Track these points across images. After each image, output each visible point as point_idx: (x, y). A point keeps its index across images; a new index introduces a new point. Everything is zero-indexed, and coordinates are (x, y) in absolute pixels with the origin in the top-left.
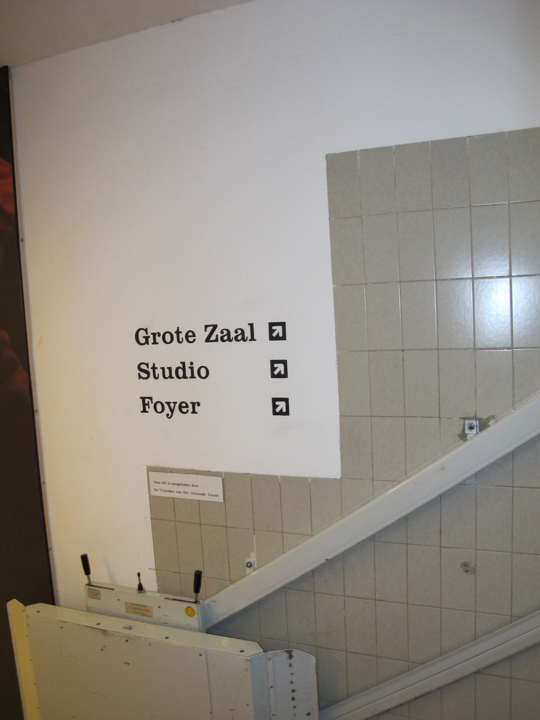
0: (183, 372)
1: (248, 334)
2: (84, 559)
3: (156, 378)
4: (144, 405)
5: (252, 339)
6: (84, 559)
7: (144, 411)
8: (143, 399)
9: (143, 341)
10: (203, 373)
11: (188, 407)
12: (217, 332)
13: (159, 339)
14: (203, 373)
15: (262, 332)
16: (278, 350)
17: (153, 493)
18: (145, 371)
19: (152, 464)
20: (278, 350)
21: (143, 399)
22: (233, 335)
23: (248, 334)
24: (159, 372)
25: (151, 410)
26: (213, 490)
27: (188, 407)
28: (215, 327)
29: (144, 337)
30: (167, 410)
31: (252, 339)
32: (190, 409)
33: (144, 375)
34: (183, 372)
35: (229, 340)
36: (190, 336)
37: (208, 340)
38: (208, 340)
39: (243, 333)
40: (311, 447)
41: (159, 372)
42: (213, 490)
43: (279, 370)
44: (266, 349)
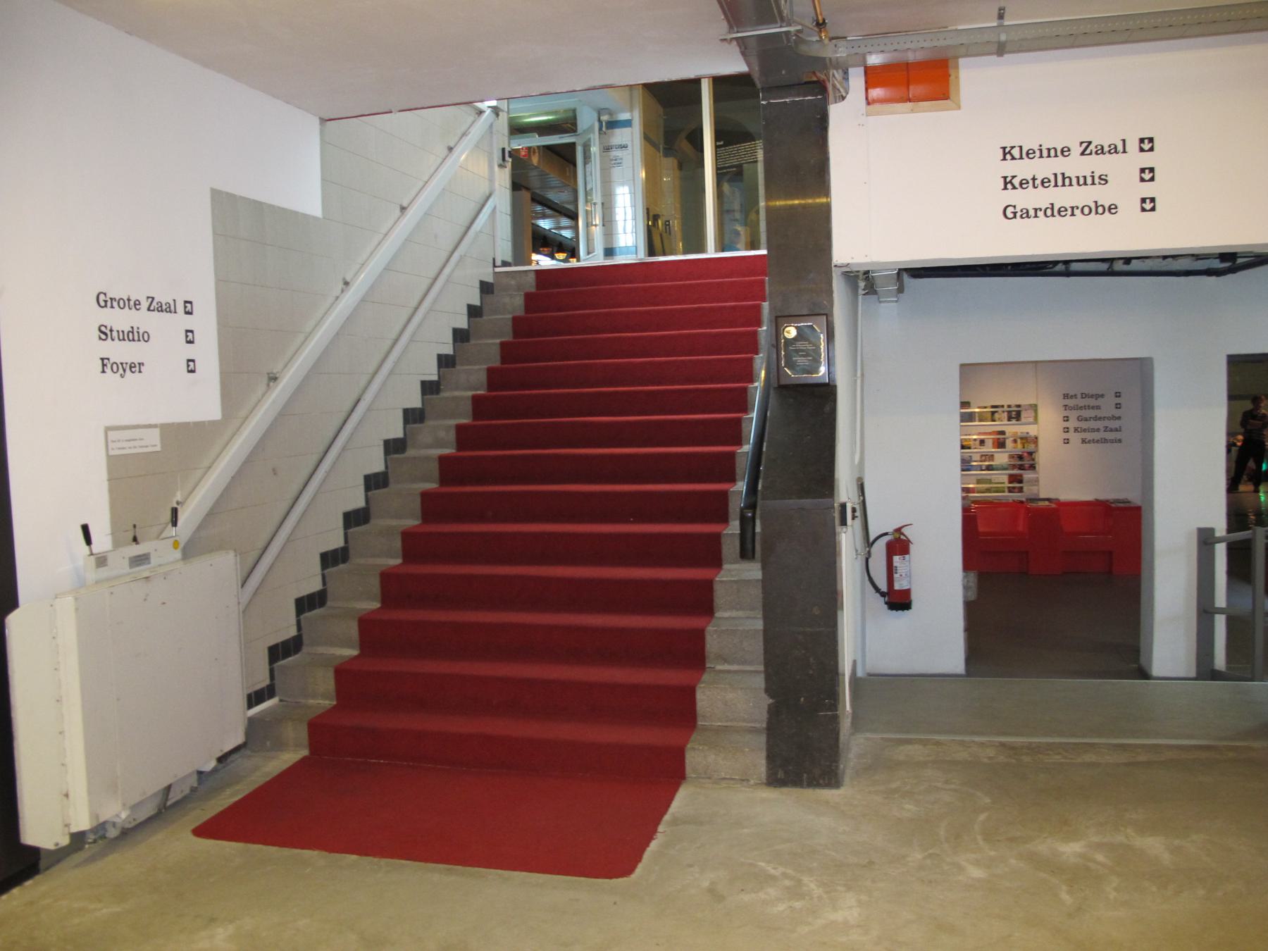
0: (132, 335)
1: (1120, 148)
2: (85, 529)
3: (1035, 187)
4: (104, 365)
5: (1124, 152)
6: (85, 529)
7: (103, 372)
8: (102, 359)
9: (102, 304)
10: (144, 337)
11: (135, 367)
12: (1092, 147)
13: (115, 304)
14: (144, 337)
15: (1133, 146)
16: (1147, 160)
17: (112, 453)
18: (105, 333)
19: (109, 423)
20: (1147, 160)
21: (102, 359)
22: (1106, 149)
23: (1120, 148)
24: (115, 334)
25: (108, 370)
26: (152, 441)
27: (135, 367)
28: (1090, 143)
29: (103, 301)
30: (121, 371)
31: (1124, 152)
32: (1069, 212)
33: (103, 337)
34: (132, 335)
35: (1103, 153)
36: (1065, 152)
37: (1083, 154)
38: (1083, 154)
39: (1102, 148)
40: (202, 401)
41: (115, 334)
42: (152, 441)
43: (1148, 174)
44: (181, 321)
